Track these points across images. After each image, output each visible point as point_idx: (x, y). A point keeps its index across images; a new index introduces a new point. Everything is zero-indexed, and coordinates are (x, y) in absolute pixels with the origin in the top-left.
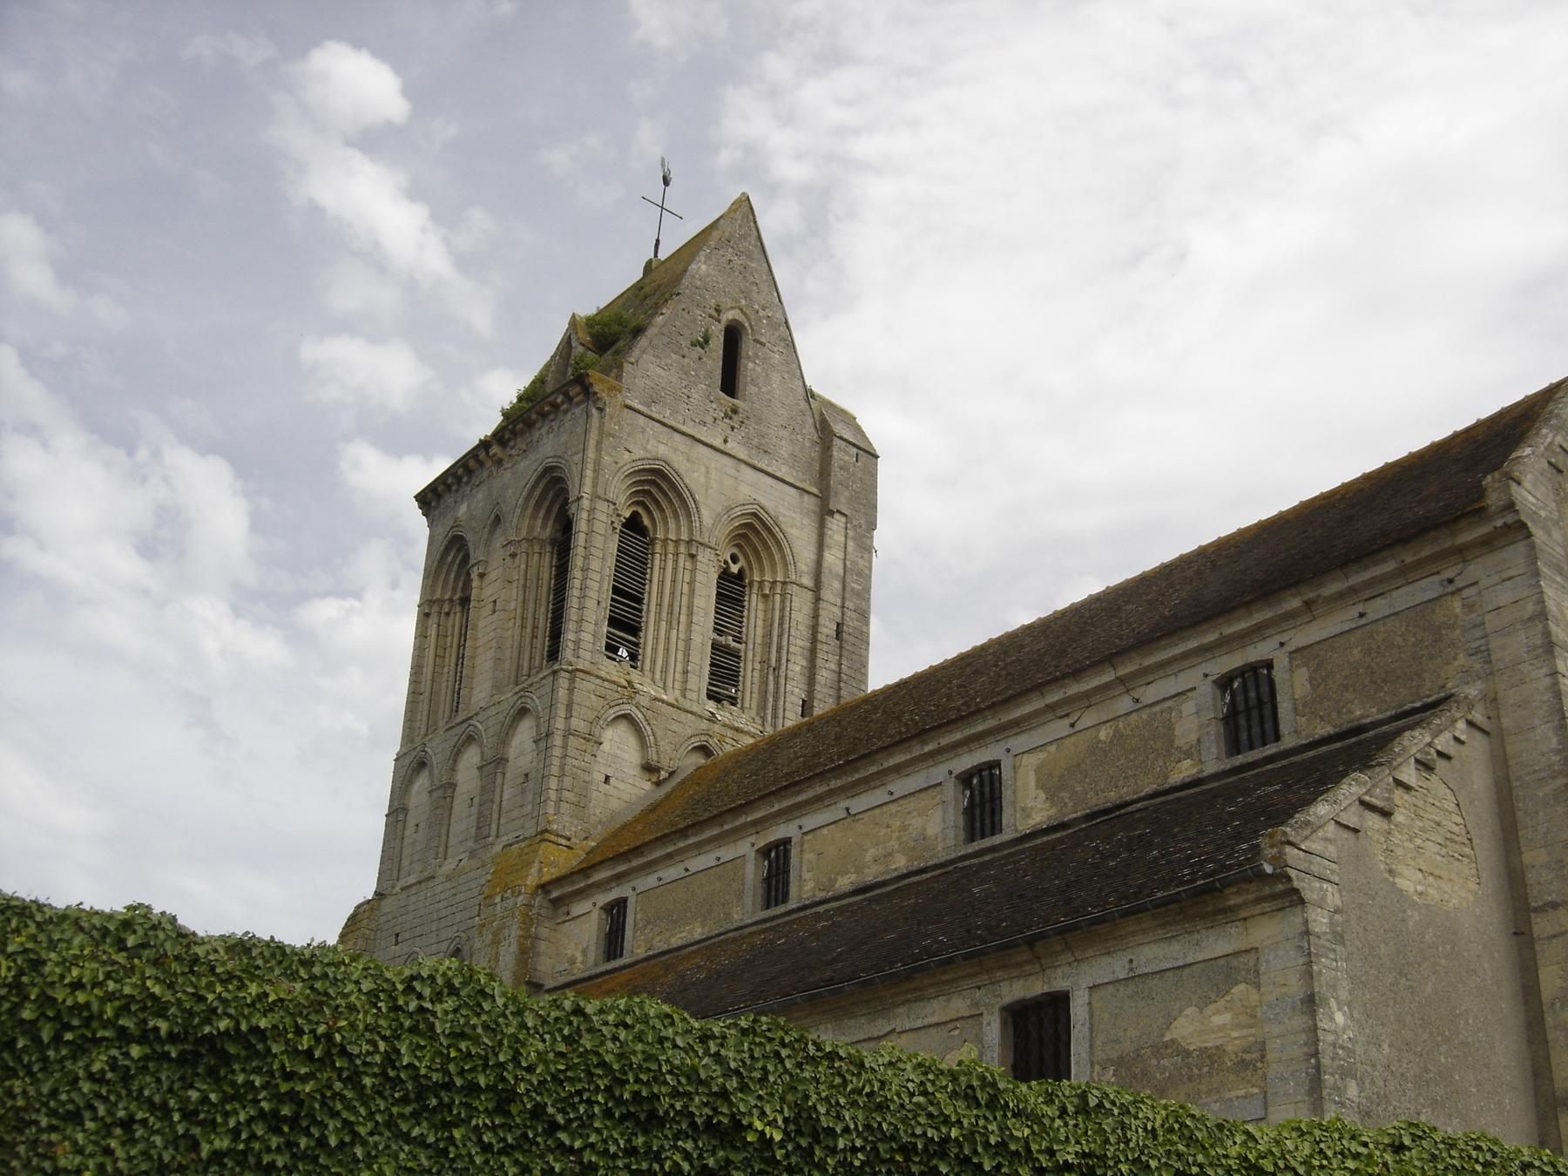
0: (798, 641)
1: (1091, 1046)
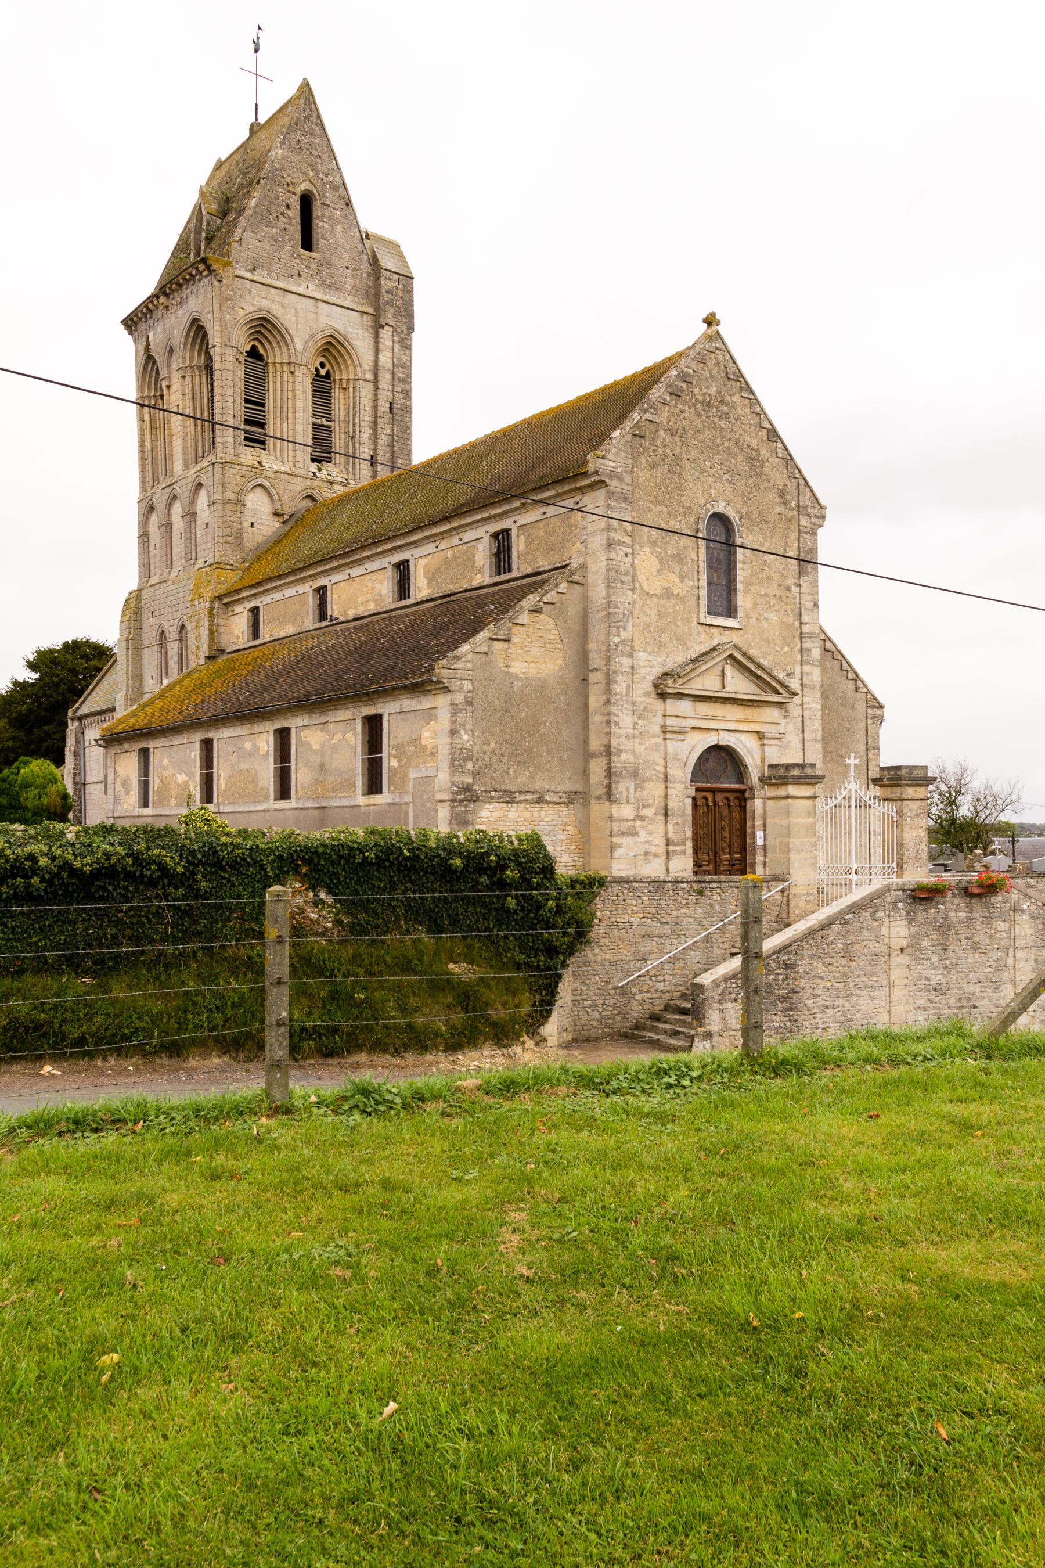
0: (366, 418)
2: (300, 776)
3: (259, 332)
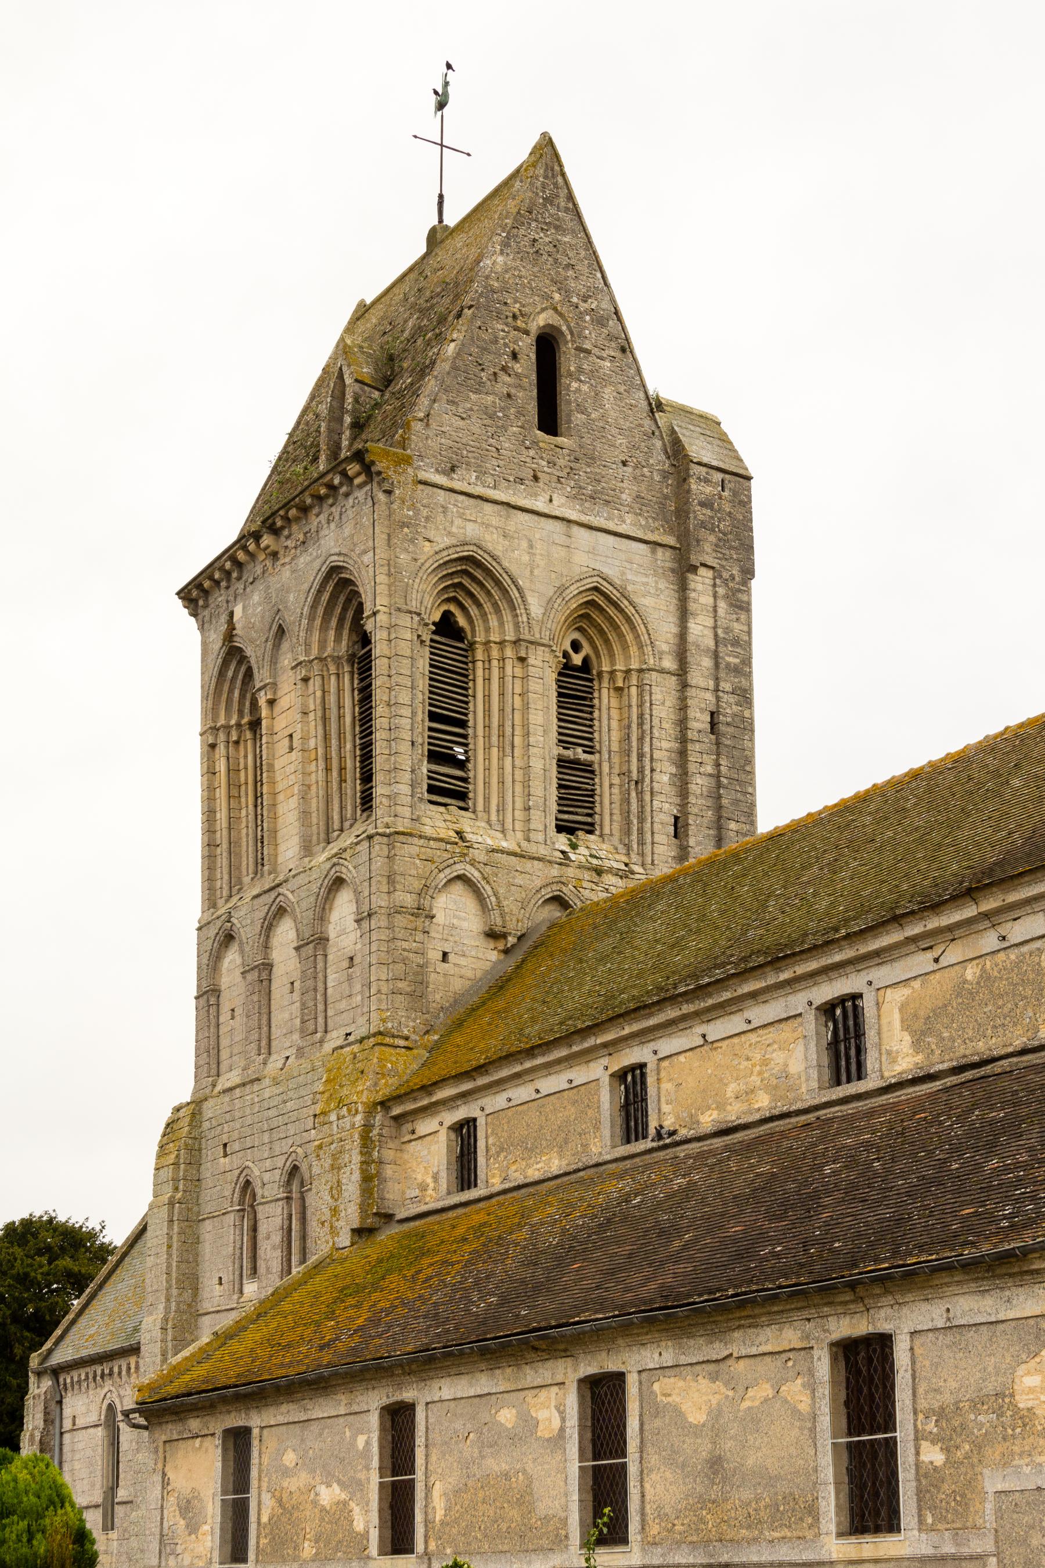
0: (664, 744)
1: (914, 1394)
3: (460, 586)
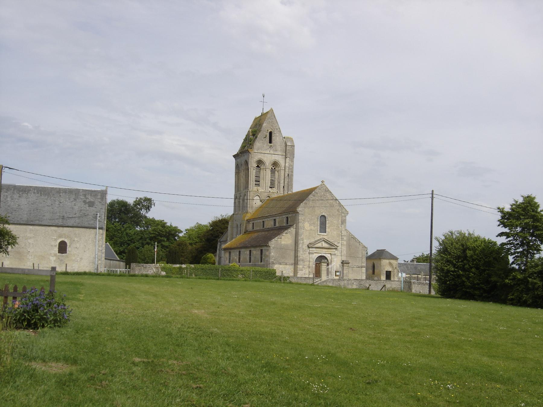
0: (282, 178)
2: (252, 259)
